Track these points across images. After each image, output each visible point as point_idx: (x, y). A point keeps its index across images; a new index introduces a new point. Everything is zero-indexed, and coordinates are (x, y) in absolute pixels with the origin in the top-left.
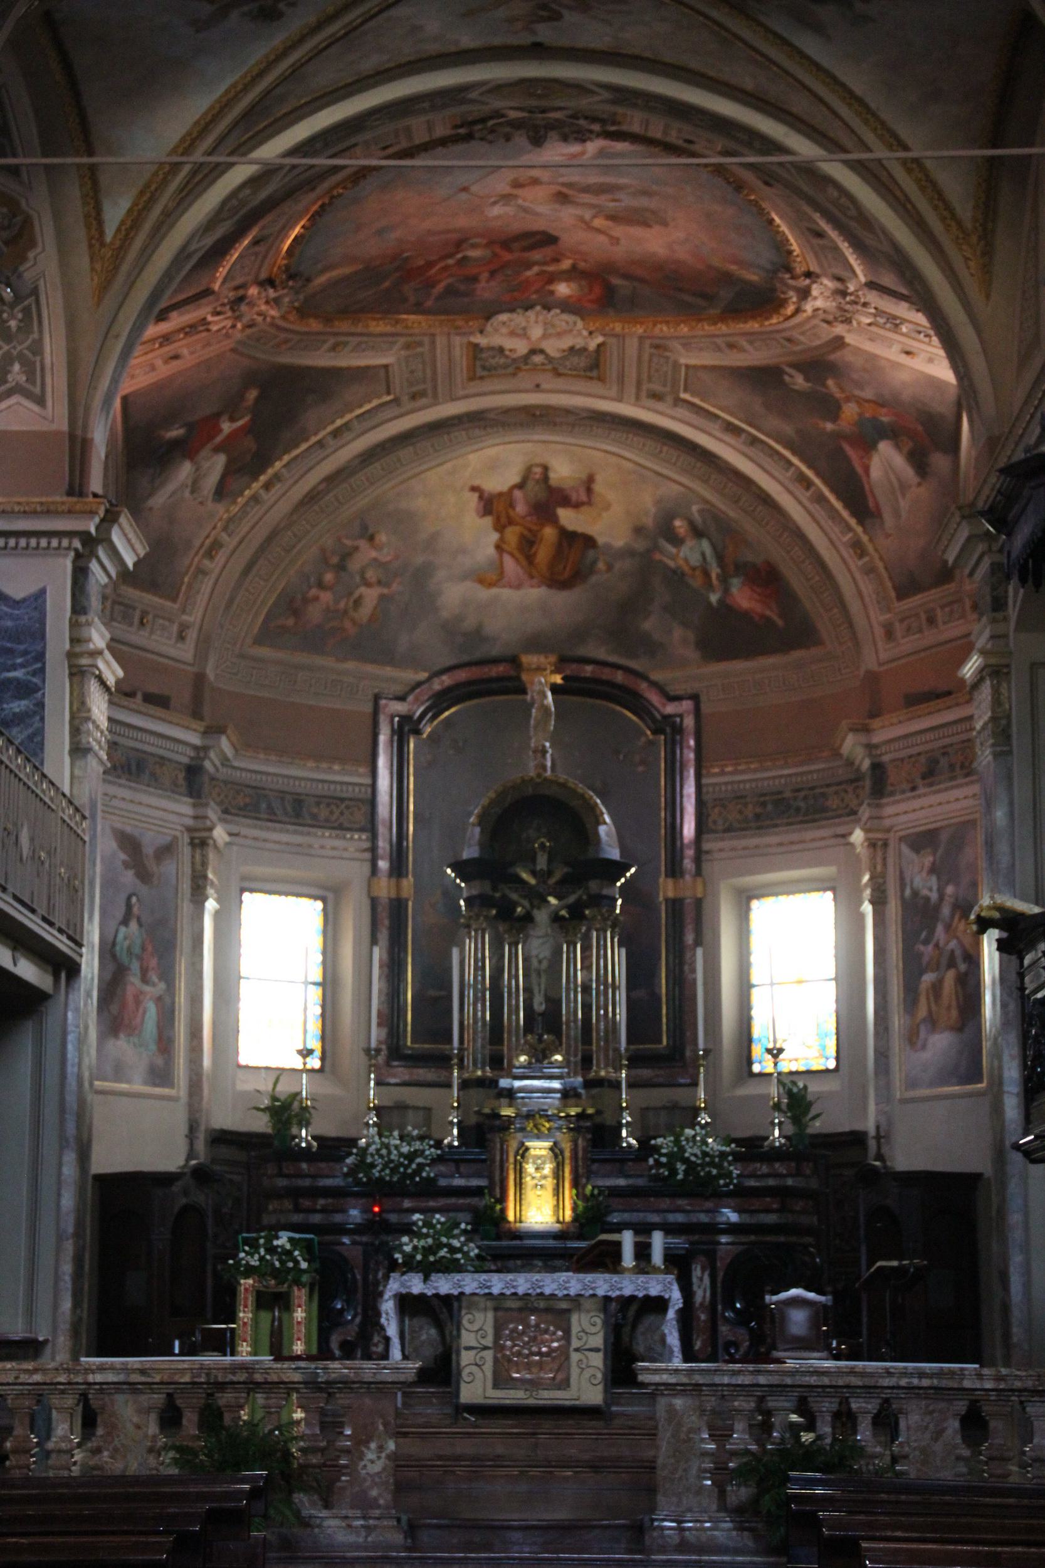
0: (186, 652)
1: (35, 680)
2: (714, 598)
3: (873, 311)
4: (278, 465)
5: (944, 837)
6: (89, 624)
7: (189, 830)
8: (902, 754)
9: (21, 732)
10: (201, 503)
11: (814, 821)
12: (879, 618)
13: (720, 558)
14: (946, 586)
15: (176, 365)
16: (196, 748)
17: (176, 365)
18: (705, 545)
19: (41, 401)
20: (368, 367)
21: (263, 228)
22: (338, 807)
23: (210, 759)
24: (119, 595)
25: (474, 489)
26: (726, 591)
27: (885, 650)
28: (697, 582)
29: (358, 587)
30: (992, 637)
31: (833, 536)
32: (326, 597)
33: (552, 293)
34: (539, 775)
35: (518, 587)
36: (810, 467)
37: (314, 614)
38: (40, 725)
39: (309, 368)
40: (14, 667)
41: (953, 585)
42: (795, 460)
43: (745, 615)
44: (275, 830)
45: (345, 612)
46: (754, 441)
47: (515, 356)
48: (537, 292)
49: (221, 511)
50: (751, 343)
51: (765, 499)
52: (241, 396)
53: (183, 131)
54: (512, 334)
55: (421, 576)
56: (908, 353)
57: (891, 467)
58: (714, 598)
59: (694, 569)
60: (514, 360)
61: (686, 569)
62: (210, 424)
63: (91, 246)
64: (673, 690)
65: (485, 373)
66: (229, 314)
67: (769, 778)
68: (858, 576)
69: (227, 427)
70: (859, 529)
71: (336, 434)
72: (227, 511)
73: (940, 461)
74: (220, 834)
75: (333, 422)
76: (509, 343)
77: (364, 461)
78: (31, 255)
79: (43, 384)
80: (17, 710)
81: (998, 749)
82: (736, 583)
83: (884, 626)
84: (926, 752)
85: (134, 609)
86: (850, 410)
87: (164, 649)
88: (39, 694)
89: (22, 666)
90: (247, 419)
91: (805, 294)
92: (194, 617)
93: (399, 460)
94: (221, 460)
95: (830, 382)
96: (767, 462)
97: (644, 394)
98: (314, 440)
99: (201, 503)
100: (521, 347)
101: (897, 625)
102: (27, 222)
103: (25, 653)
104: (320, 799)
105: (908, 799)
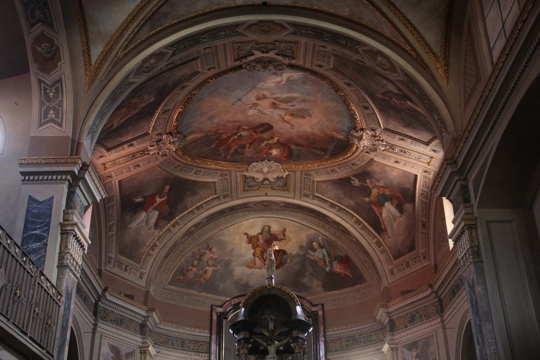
0: (142, 283)
1: (44, 234)
2: (327, 269)
3: (385, 143)
4: (177, 218)
5: (420, 343)
6: (73, 213)
7: (140, 347)
8: (401, 315)
9: (35, 257)
10: (149, 229)
11: (368, 345)
12: (387, 267)
13: (329, 255)
14: (413, 252)
15: (138, 170)
16: (144, 317)
17: (138, 170)
18: (324, 250)
19: (60, 125)
20: (208, 182)
21: (165, 105)
22: (197, 344)
23: (149, 321)
24: (117, 258)
25: (245, 234)
26: (332, 266)
27: (390, 279)
28: (321, 264)
29: (206, 267)
30: (466, 214)
31: (369, 241)
32: (194, 269)
33: (271, 153)
34: (269, 285)
35: (260, 269)
36: (360, 216)
37: (190, 275)
38: (44, 253)
39: (187, 180)
40: (36, 229)
41: (415, 251)
42: (355, 215)
43: (339, 274)
44: (174, 352)
45: (201, 275)
46: (341, 209)
47: (258, 181)
48: (265, 154)
49: (156, 233)
50: (339, 168)
51: (345, 232)
52: (163, 188)
53: (123, 19)
54: (258, 171)
55: (227, 264)
56: (396, 162)
57: (390, 212)
58: (327, 269)
59: (320, 259)
60: (258, 183)
61: (317, 260)
62: (152, 197)
63: (85, 65)
64: (315, 302)
65: (249, 189)
66: (156, 147)
67: (350, 331)
68: (379, 254)
69: (158, 200)
70: (379, 237)
71: (198, 208)
72: (159, 233)
73: (408, 207)
74: (152, 349)
75: (196, 204)
76: (256, 176)
77: (208, 221)
78: (59, 64)
79: (62, 118)
80: (35, 247)
81: (476, 260)
82: (335, 263)
83: (390, 271)
84: (410, 313)
85: (123, 264)
86: (375, 192)
87: (134, 281)
88: (45, 240)
89: (40, 228)
90: (166, 198)
91: (360, 138)
92: (146, 271)
93: (220, 222)
94: (157, 213)
95: (368, 181)
96: (345, 217)
97: (302, 195)
98: (190, 210)
99: (149, 229)
100: (260, 177)
101: (395, 269)
102: (58, 49)
103: (42, 223)
104: (191, 341)
105: (404, 331)
